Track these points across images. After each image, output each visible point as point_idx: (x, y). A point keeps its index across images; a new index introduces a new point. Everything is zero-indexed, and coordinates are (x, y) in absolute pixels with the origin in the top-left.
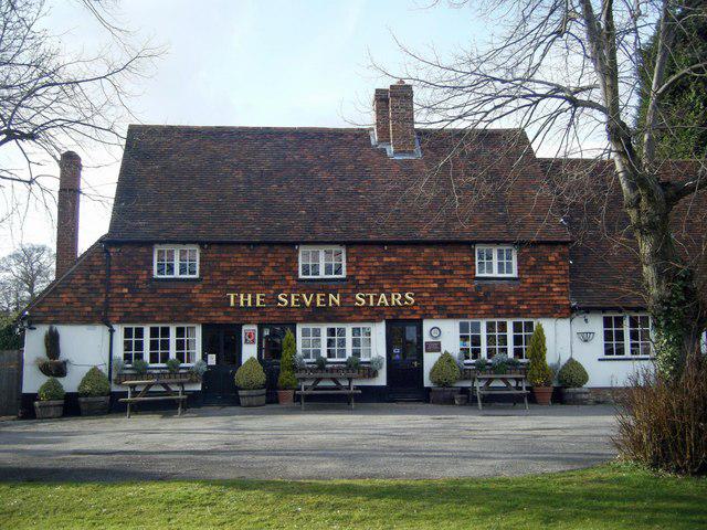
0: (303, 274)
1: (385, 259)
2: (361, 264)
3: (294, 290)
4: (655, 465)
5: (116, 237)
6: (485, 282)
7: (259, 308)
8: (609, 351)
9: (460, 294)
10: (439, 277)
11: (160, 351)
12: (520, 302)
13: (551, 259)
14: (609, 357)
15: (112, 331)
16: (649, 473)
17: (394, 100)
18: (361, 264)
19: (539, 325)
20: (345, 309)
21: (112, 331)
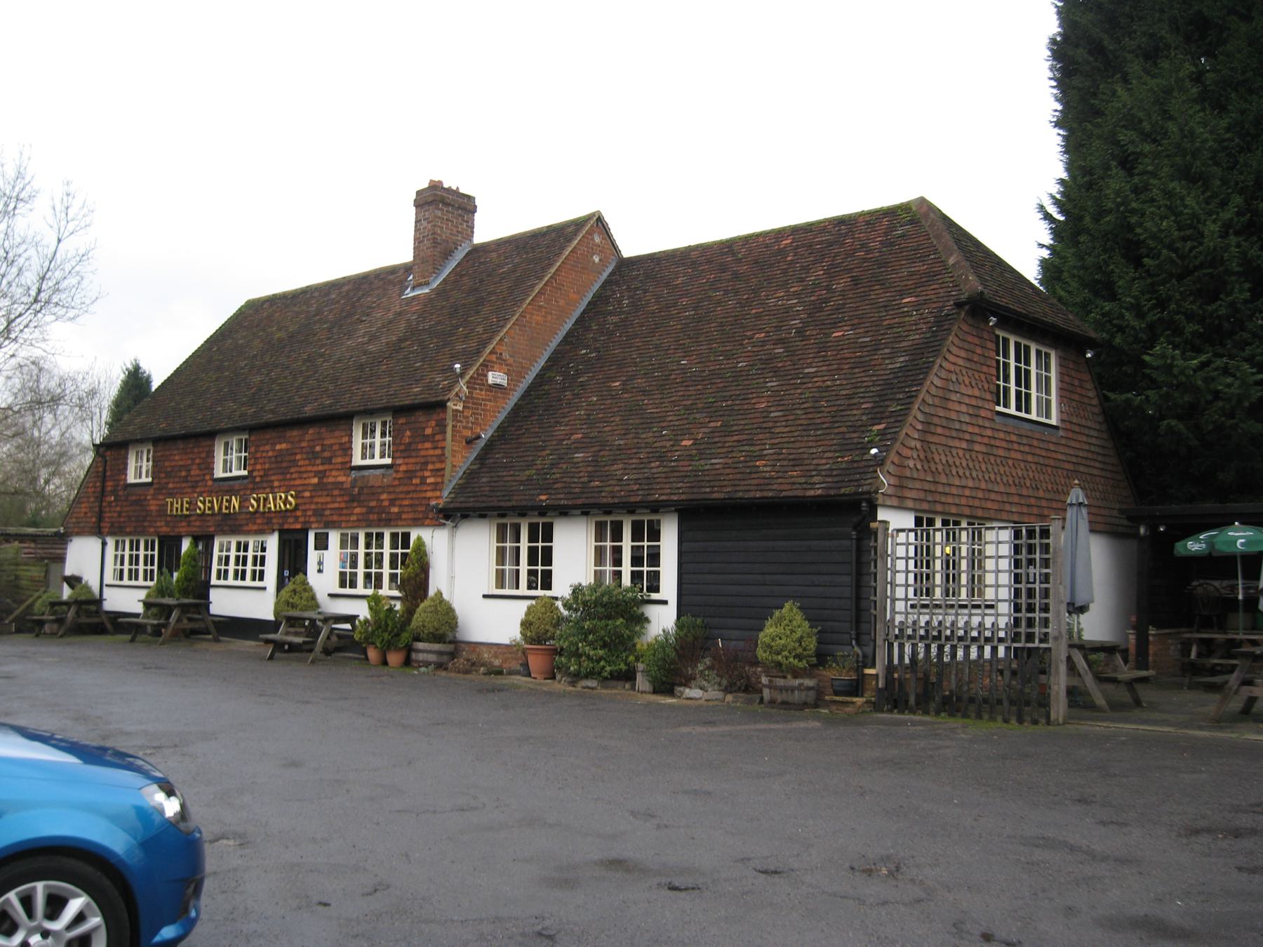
0: (225, 471)
1: (278, 447)
2: (259, 455)
3: (210, 493)
4: (726, 690)
5: (205, 443)
6: (366, 473)
7: (187, 516)
8: (500, 580)
9: (336, 492)
10: (321, 468)
11: (645, 569)
12: (392, 502)
13: (428, 431)
14: (348, 591)
15: (104, 544)
16: (720, 695)
17: (443, 208)
18: (259, 455)
19: (419, 539)
20: (243, 516)
21: (104, 544)
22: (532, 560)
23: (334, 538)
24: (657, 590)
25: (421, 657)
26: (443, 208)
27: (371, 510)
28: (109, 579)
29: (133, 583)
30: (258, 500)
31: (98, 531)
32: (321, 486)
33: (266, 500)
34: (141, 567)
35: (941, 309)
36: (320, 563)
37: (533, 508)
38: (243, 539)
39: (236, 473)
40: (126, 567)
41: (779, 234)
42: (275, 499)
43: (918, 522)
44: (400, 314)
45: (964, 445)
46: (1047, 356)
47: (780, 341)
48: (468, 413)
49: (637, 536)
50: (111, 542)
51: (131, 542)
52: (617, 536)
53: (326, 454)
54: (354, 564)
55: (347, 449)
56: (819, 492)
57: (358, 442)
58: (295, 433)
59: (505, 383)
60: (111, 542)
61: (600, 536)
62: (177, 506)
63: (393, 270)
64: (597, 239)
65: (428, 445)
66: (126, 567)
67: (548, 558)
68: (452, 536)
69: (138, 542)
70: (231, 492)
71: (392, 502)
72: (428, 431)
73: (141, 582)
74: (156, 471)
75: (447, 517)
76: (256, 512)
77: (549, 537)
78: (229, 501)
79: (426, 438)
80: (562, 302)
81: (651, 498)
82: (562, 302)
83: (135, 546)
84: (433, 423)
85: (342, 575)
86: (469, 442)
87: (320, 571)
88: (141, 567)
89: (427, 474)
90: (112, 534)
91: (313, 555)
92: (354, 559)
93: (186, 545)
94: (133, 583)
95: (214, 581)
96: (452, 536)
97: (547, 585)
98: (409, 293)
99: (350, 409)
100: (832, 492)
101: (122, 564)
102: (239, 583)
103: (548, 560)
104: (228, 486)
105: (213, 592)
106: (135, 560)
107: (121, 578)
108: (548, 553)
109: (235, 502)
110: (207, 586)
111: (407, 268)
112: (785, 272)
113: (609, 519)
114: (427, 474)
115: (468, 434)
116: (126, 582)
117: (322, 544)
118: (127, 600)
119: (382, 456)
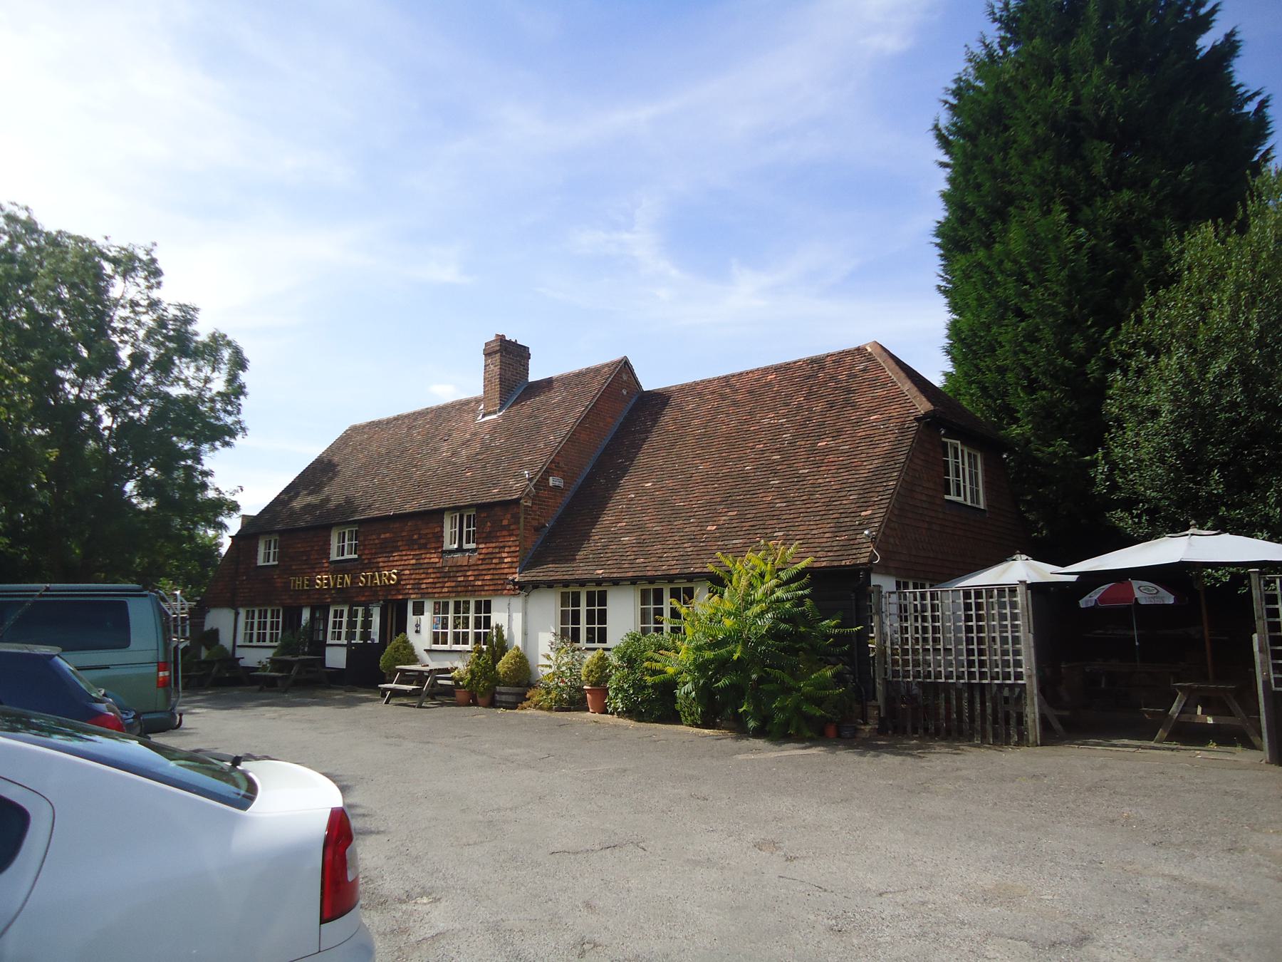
12: (477, 577)
13: (505, 522)
15: (237, 614)
17: (508, 357)
22: (590, 620)
23: (429, 606)
24: (605, 642)
25: (504, 698)
26: (508, 357)
27: (459, 584)
28: (240, 642)
29: (261, 644)
30: (366, 577)
31: (233, 605)
32: (417, 566)
33: (373, 576)
34: (268, 631)
35: (903, 423)
36: (418, 625)
37: (591, 581)
38: (339, 608)
39: (347, 556)
40: (255, 631)
41: (766, 371)
42: (380, 576)
43: (898, 584)
44: (475, 434)
45: (926, 526)
46: (975, 457)
47: (778, 451)
48: (535, 508)
49: (590, 602)
50: (243, 612)
51: (260, 612)
52: (576, 603)
53: (422, 541)
54: (445, 626)
55: (439, 537)
56: (824, 564)
57: (334, 544)
58: (397, 525)
59: (562, 485)
60: (243, 612)
61: (644, 601)
62: (299, 582)
63: (467, 402)
64: (625, 378)
65: (505, 533)
66: (255, 631)
67: (603, 617)
68: (526, 602)
69: (266, 612)
70: (344, 571)
71: (477, 577)
72: (505, 522)
73: (268, 643)
74: (281, 556)
75: (521, 588)
76: (366, 586)
77: (603, 601)
78: (343, 579)
79: (504, 528)
80: (601, 424)
81: (686, 571)
82: (601, 424)
83: (263, 615)
84: (509, 516)
85: (436, 634)
86: (537, 529)
87: (417, 632)
88: (268, 631)
89: (504, 555)
90: (242, 606)
91: (411, 619)
92: (576, 616)
93: (306, 615)
94: (261, 644)
95: (329, 641)
96: (526, 602)
97: (603, 639)
98: (480, 419)
99: (442, 506)
100: (836, 564)
101: (252, 629)
102: (337, 642)
103: (603, 619)
104: (340, 568)
105: (328, 650)
106: (262, 625)
107: (251, 641)
108: (603, 614)
109: (347, 579)
110: (323, 645)
111: (477, 401)
112: (773, 399)
113: (652, 587)
114: (504, 555)
115: (535, 523)
116: (255, 643)
117: (419, 610)
118: (255, 657)
119: (468, 542)
